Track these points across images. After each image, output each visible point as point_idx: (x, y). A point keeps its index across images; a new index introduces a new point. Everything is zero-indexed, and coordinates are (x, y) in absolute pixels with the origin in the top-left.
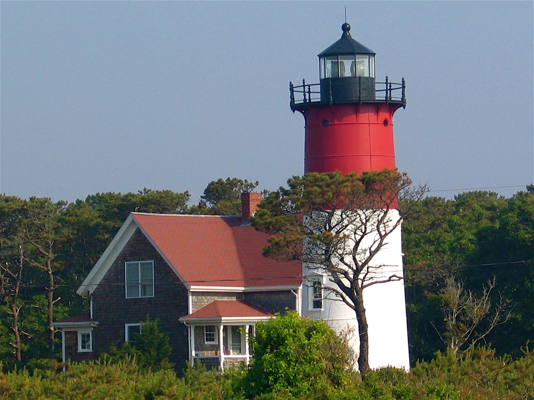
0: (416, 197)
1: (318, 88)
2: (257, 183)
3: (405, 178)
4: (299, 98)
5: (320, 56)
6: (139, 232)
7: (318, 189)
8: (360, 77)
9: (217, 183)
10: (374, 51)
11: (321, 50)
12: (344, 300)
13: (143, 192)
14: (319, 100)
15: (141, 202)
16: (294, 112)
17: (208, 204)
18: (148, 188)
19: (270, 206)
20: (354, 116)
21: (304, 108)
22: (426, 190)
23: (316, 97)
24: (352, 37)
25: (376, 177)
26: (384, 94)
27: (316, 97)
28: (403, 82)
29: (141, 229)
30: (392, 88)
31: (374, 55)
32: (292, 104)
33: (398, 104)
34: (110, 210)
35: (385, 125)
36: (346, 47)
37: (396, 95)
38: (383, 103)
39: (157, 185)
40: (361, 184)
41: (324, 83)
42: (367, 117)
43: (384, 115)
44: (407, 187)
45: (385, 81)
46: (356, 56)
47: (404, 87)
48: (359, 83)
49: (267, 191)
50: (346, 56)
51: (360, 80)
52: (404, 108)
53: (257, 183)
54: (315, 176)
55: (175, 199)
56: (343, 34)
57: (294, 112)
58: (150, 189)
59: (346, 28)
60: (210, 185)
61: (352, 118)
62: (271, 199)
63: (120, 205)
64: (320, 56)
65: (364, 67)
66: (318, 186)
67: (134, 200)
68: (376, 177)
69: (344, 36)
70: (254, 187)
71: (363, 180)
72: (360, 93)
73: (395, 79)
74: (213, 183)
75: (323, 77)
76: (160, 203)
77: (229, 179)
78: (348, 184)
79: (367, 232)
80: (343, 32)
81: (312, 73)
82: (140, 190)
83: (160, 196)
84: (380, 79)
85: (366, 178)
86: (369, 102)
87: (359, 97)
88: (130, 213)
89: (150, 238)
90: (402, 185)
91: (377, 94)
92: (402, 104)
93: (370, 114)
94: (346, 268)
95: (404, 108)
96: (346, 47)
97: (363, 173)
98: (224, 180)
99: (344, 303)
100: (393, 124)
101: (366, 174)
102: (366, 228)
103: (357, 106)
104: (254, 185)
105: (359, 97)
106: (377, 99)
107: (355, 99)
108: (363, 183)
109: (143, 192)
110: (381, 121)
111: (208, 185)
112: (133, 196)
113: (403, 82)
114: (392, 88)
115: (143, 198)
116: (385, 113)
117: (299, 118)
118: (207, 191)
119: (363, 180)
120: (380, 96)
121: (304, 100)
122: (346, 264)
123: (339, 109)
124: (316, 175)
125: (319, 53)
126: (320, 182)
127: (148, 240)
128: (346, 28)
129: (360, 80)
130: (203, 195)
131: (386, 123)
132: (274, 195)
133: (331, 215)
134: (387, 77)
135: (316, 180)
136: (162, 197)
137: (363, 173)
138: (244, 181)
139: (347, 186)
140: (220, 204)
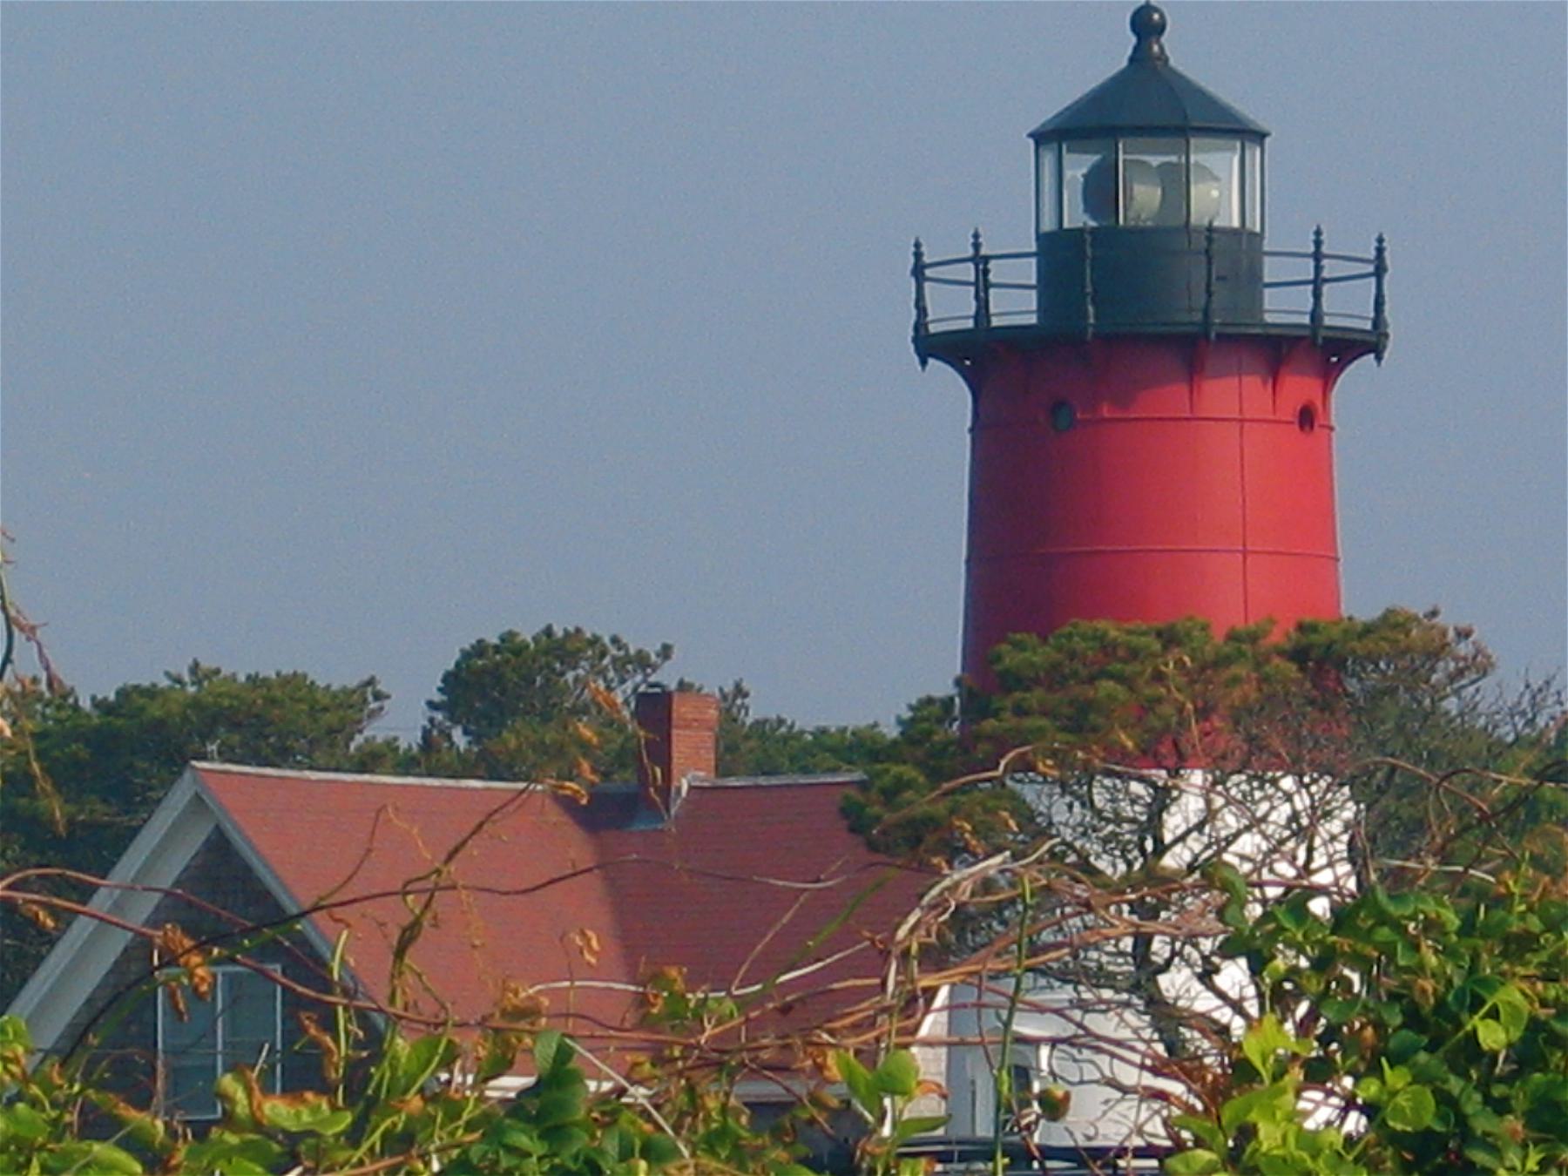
0: (1508, 728)
1: (1028, 271)
2: (666, 652)
3: (1464, 649)
4: (952, 310)
5: (1040, 138)
6: (220, 847)
7: (1120, 691)
8: (1210, 229)
9: (497, 649)
10: (1262, 123)
11: (1047, 110)
12: (1122, 1059)
13: (187, 678)
14: (1032, 320)
15: (185, 719)
16: (924, 363)
17: (457, 735)
18: (207, 664)
19: (919, 753)
20: (1184, 388)
21: (975, 352)
22: (1550, 701)
23: (1016, 306)
24: (1172, 62)
25: (1355, 644)
26: (1303, 298)
27: (1016, 306)
28: (1380, 251)
29: (235, 838)
30: (1325, 274)
31: (1260, 137)
32: (922, 332)
33: (1364, 342)
34: (57, 753)
35: (1302, 427)
36: (1144, 106)
37: (1347, 308)
38: (1300, 338)
39: (248, 655)
40: (1291, 669)
41: (1058, 253)
42: (1233, 393)
43: (1298, 387)
44: (1472, 689)
45: (1312, 249)
46: (1192, 141)
47: (1380, 271)
48: (1207, 251)
49: (691, 686)
50: (1163, 141)
51: (1210, 240)
52: (1379, 358)
53: (666, 652)
54: (1101, 638)
55: (326, 709)
56: (1136, 49)
57: (924, 363)
58: (214, 666)
59: (1146, 25)
60: (466, 655)
61: (1172, 397)
62: (925, 725)
63: (97, 730)
64: (1040, 138)
65: (1219, 190)
66: (1119, 678)
67: (155, 711)
68: (1355, 644)
69: (1140, 56)
70: (655, 668)
71: (1299, 655)
72: (1209, 294)
73: (1349, 243)
74: (480, 649)
75: (1048, 225)
76: (281, 722)
77: (548, 631)
78: (1240, 670)
79: (1314, 866)
80: (1134, 40)
81: (1001, 212)
82: (173, 671)
83: (264, 698)
84: (1285, 239)
85: (1310, 646)
86: (1243, 330)
87: (1206, 312)
88: (186, 762)
89: (272, 872)
90: (1452, 678)
91: (1270, 298)
92: (1372, 343)
93: (1246, 379)
94: (1225, 1015)
95: (1379, 358)
96: (1144, 106)
97: (1301, 627)
98: (527, 636)
99: (14, 656)
100: (1334, 422)
101: (1314, 629)
102: (1310, 850)
103: (1193, 350)
104: (653, 657)
105: (1206, 312)
106: (1269, 318)
107: (1185, 318)
108: (1302, 669)
109: (187, 678)
110: (1289, 410)
111: (457, 656)
112: (151, 693)
113: (1380, 251)
114: (1325, 274)
115: (195, 704)
116: (1307, 380)
117: (948, 395)
118: (451, 681)
119: (1299, 655)
120: (1284, 307)
121: (976, 318)
122: (1221, 995)
123: (1111, 358)
124: (1105, 634)
125: (1034, 126)
126: (1125, 661)
127: (259, 880)
128: (1146, 25)
129: (1210, 240)
130: (438, 697)
131: (1307, 418)
132: (936, 710)
133: (1163, 799)
134: (1318, 233)
135: (1108, 648)
136: (273, 702)
137: (1301, 627)
138: (606, 640)
139: (1236, 680)
140: (518, 734)
